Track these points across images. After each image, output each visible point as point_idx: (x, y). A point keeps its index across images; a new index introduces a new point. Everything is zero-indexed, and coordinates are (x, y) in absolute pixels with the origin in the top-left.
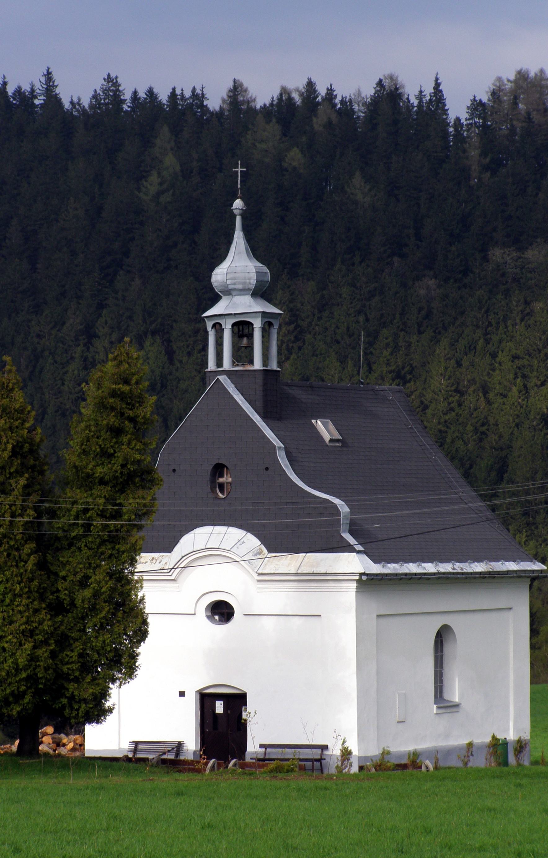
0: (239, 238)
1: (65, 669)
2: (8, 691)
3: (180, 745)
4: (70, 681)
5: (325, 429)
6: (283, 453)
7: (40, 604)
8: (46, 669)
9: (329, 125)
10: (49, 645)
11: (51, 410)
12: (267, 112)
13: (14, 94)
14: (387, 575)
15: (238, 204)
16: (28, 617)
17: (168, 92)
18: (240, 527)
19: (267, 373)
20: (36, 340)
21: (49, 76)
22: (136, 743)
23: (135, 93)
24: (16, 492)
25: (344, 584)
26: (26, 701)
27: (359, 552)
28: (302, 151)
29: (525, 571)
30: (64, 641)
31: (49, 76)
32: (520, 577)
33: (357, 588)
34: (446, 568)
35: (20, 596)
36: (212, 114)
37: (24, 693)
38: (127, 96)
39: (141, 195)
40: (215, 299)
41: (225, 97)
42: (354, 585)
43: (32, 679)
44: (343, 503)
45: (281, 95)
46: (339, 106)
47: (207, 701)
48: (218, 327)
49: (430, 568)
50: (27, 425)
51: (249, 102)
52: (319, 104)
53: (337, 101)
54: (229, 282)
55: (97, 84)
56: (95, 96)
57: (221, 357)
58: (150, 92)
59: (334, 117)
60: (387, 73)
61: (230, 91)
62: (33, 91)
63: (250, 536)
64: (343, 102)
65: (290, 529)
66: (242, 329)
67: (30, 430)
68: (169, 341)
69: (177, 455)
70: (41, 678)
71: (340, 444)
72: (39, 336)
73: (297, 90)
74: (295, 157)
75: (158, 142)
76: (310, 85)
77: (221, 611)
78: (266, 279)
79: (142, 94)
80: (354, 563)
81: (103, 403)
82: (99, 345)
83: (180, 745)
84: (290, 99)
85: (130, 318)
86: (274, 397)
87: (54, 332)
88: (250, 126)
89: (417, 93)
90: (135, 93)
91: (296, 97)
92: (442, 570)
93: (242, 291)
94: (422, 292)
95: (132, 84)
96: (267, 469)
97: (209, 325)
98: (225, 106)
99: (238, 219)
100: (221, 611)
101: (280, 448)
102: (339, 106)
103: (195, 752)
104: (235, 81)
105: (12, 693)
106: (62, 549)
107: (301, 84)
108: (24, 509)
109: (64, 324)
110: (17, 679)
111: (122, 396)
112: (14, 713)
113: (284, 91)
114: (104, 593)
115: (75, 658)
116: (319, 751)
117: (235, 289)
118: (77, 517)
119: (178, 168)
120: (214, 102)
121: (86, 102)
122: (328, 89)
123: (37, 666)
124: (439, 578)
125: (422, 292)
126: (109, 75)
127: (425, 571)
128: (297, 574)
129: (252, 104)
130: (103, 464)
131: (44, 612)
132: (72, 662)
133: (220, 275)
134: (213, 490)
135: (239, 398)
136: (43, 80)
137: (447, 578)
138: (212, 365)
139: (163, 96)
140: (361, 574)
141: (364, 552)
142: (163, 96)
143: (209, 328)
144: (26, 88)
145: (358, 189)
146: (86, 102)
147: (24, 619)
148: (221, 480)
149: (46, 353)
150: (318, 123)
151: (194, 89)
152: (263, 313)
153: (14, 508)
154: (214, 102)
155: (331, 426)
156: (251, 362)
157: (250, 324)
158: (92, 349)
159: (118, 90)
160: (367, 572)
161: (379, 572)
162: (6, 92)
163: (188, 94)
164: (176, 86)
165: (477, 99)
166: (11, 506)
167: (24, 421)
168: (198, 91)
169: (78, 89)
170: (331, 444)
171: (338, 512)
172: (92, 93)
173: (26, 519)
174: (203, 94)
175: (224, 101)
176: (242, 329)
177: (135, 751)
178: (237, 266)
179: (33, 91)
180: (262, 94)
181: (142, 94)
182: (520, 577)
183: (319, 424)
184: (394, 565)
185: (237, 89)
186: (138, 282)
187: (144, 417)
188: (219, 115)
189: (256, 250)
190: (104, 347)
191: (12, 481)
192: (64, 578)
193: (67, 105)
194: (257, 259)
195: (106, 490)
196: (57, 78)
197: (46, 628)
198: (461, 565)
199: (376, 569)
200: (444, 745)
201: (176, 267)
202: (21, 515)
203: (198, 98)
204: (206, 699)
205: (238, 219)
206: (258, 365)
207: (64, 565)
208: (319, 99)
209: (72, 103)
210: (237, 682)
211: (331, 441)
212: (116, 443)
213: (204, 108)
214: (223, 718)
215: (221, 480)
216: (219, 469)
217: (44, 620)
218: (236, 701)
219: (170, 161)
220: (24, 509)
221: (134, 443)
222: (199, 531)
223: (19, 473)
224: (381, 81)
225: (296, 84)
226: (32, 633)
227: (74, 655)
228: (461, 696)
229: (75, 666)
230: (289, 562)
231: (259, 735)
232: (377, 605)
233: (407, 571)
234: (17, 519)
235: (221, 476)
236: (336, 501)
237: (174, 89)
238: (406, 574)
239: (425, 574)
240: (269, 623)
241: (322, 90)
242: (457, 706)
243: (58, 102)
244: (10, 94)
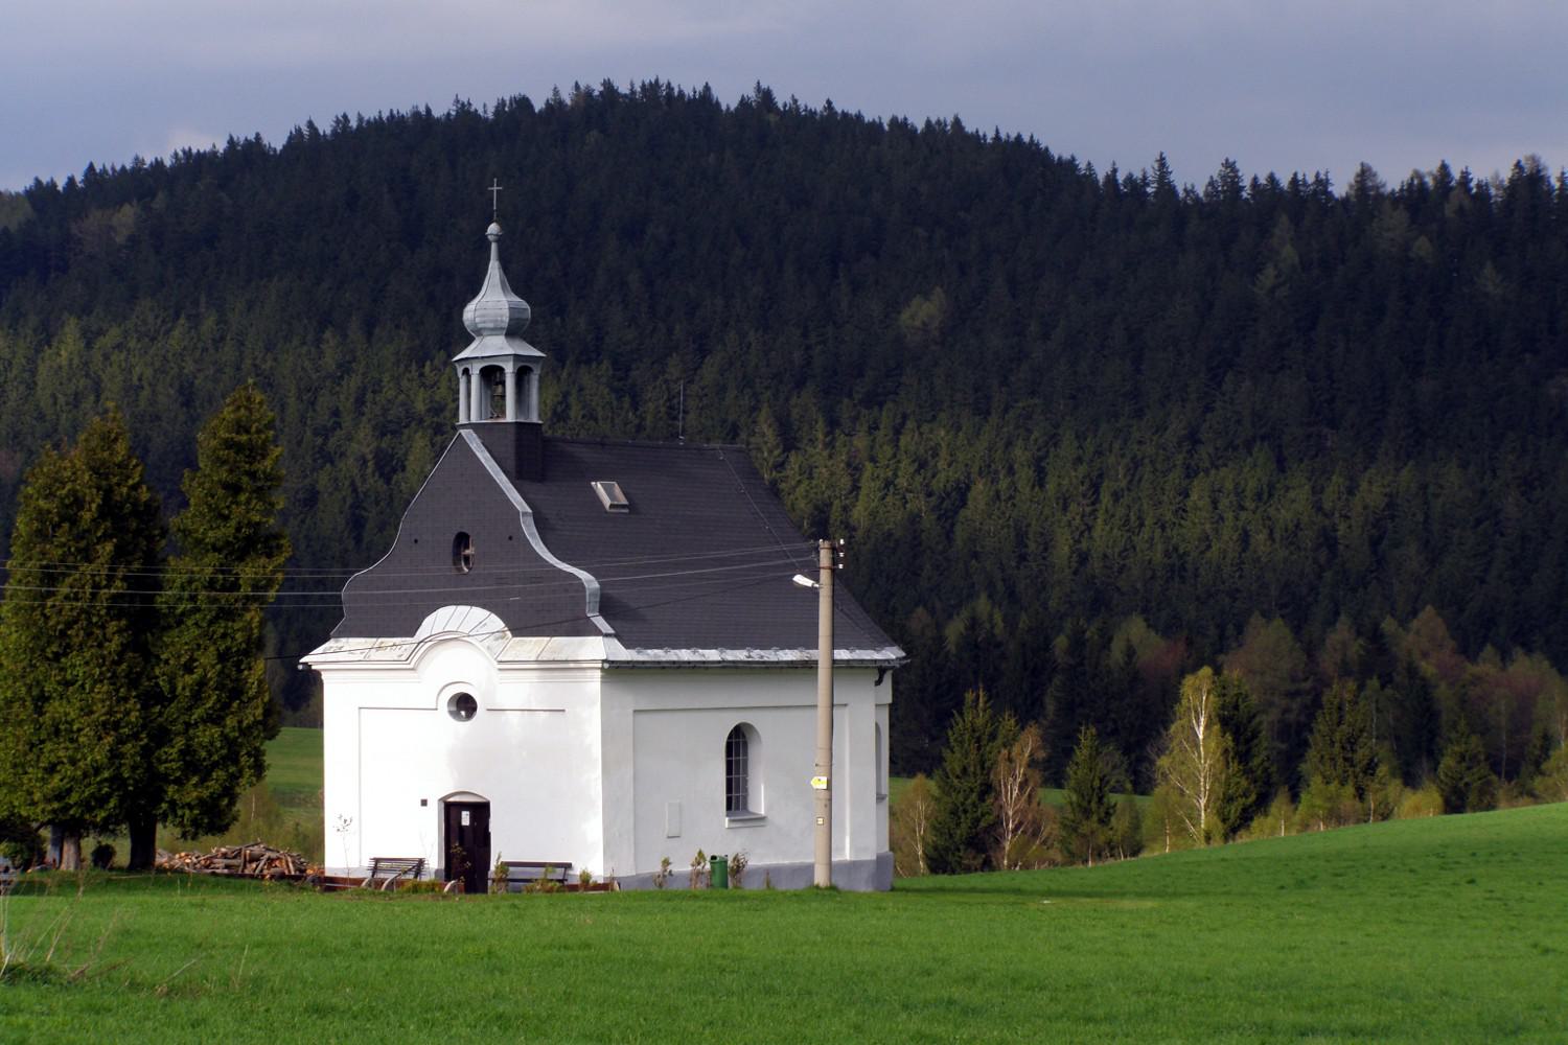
0: (494, 269)
1: (162, 768)
2: (87, 793)
3: (421, 862)
4: (170, 783)
5: (606, 493)
6: (531, 520)
7: (129, 690)
8: (134, 768)
9: (1461, 210)
10: (141, 740)
11: (1148, 522)
12: (1396, 199)
13: (1125, 181)
14: (643, 662)
15: (493, 228)
16: (111, 707)
17: (1289, 177)
18: (484, 607)
19: (519, 426)
20: (1135, 447)
21: (1162, 162)
22: (377, 861)
23: (1255, 179)
24: (102, 560)
25: (589, 673)
26: (111, 805)
27: (607, 635)
28: (1431, 241)
29: (862, 661)
30: (162, 736)
31: (1162, 162)
32: (852, 667)
33: (602, 677)
34: (740, 655)
35: (101, 681)
36: (1337, 200)
37: (108, 796)
38: (1246, 182)
39: (1255, 290)
40: (467, 339)
41: (1353, 182)
42: (598, 674)
43: (117, 781)
44: (592, 578)
45: (1412, 179)
46: (1474, 190)
47: (453, 811)
48: (466, 372)
49: (712, 655)
50: (131, 482)
51: (1378, 188)
52: (1452, 188)
53: (1473, 184)
54: (477, 320)
55: (1215, 170)
56: (1212, 183)
57: (471, 406)
58: (1272, 178)
59: (1467, 203)
60: (1529, 153)
61: (1358, 176)
62: (1145, 178)
63: (494, 617)
64: (1479, 186)
65: (536, 611)
66: (491, 375)
67: (135, 487)
68: (1280, 446)
69: (424, 520)
70: (129, 778)
71: (626, 511)
72: (1140, 442)
73: (1430, 174)
74: (1423, 247)
75: (1277, 231)
76: (1444, 168)
77: (464, 705)
78: (524, 316)
79: (1262, 181)
80: (597, 648)
81: (218, 458)
82: (1204, 452)
83: (421, 862)
84: (1422, 184)
85: (1239, 422)
86: (531, 456)
87: (1155, 438)
88: (1376, 213)
89: (1559, 175)
90: (1255, 179)
91: (1430, 181)
92: (730, 658)
93: (495, 331)
94: (1553, 391)
95: (1252, 171)
96: (510, 538)
97: (460, 371)
98: (1353, 192)
99: (494, 246)
100: (464, 705)
101: (525, 514)
102: (1474, 190)
103: (437, 872)
104: (1362, 164)
105: (92, 795)
106: (170, 627)
107: (1434, 167)
108: (110, 579)
109: (1166, 429)
110: (98, 779)
111: (238, 447)
112: (98, 819)
113: (1417, 175)
114: (211, 679)
115: (175, 756)
116: (560, 871)
117: (485, 329)
118: (183, 588)
119: (1297, 260)
120: (1340, 188)
121: (1201, 191)
122: (1462, 173)
123: (121, 765)
124: (724, 667)
125: (1553, 391)
126: (1227, 160)
127: (703, 659)
128: (537, 661)
129: (1382, 190)
130: (218, 527)
131: (132, 701)
132: (173, 760)
133: (471, 313)
134: (456, 562)
135: (483, 456)
136: (1156, 166)
137: (737, 668)
138: (462, 420)
139: (1284, 182)
140: (604, 661)
141: (616, 636)
142: (1284, 182)
143: (460, 375)
144: (1138, 175)
145: (1490, 281)
146: (1201, 191)
147: (106, 709)
148: (467, 552)
149: (1147, 461)
150: (1449, 210)
151: (1317, 175)
152: (515, 355)
153: (97, 579)
154: (1340, 188)
155: (617, 490)
156: (503, 413)
157: (501, 370)
158: (1196, 456)
159: (1236, 176)
160: (611, 659)
161: (629, 659)
162: (1116, 180)
163: (1311, 179)
164: (1275, 171)
165: (582, 87)
166: (93, 576)
167: (128, 477)
168: (1322, 177)
169: (1193, 176)
170: (613, 510)
171: (580, 586)
172: (1207, 180)
173: (113, 591)
174: (1327, 180)
175: (1351, 186)
176: (491, 375)
177: (375, 870)
178: (492, 302)
179: (1145, 178)
180: (1393, 178)
181: (1262, 181)
182: (852, 667)
183: (599, 487)
184: (656, 651)
185: (1365, 173)
186: (1248, 383)
187: (264, 472)
188: (1345, 201)
189: (516, 282)
190: (1209, 455)
191: (98, 547)
192: (167, 662)
193: (1182, 194)
194: (516, 291)
195: (213, 558)
196: (1171, 164)
197: (133, 720)
198: (762, 653)
199: (624, 654)
200: (786, 862)
201: (1290, 368)
202: (108, 586)
203: (1322, 183)
204: (451, 809)
205: (494, 246)
206: (510, 416)
207: (167, 646)
208: (1453, 183)
209: (1185, 190)
210: (481, 791)
211: (612, 506)
212: (232, 503)
213: (1329, 195)
214: (466, 829)
215: (467, 552)
216: (462, 540)
217: (131, 711)
218: (481, 810)
219: (1289, 253)
220: (110, 579)
221: (254, 501)
222: (441, 611)
223: (106, 537)
224: (1519, 162)
225: (1429, 167)
226: (116, 726)
227: (174, 752)
228: (768, 808)
229: (174, 765)
230: (533, 647)
231: (506, 845)
232: (629, 699)
233: (675, 658)
234: (103, 591)
235: (467, 547)
236: (583, 575)
237: (1295, 174)
238: (674, 662)
239: (704, 662)
240: (514, 717)
241: (1456, 174)
242: (762, 819)
243: (1172, 190)
244: (1120, 181)
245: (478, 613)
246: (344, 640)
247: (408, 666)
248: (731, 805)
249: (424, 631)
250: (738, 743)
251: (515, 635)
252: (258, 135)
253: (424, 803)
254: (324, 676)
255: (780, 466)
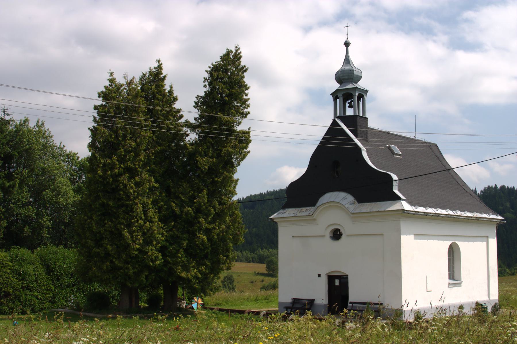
204: (331, 278)
218: (344, 280)
231: (355, 295)
245: (343, 194)
246: (286, 209)
247: (311, 219)
248: (452, 276)
249: (318, 204)
250: (453, 253)
251: (359, 202)
252: (496, 185)
253: (319, 276)
254: (279, 224)
255: (229, 146)
